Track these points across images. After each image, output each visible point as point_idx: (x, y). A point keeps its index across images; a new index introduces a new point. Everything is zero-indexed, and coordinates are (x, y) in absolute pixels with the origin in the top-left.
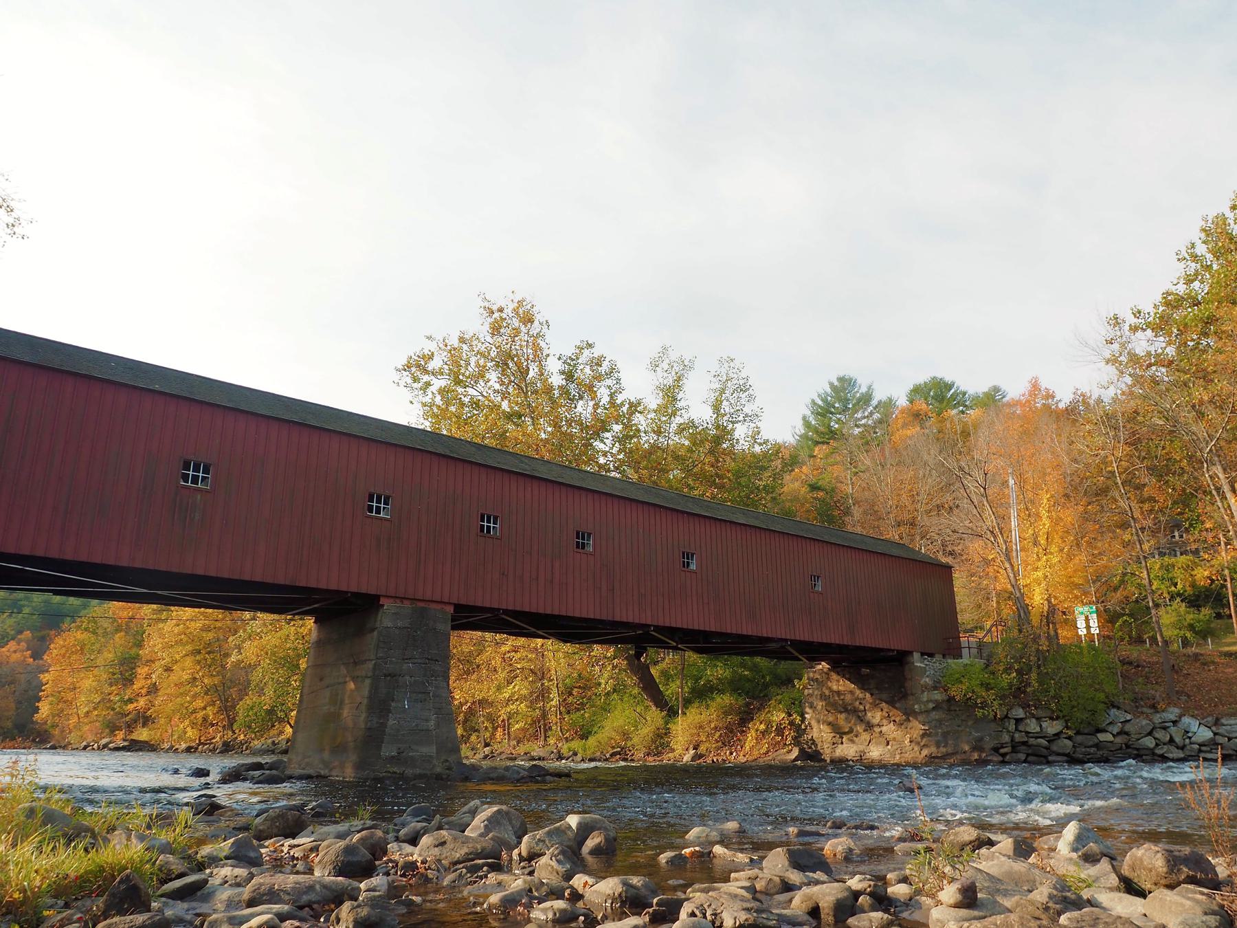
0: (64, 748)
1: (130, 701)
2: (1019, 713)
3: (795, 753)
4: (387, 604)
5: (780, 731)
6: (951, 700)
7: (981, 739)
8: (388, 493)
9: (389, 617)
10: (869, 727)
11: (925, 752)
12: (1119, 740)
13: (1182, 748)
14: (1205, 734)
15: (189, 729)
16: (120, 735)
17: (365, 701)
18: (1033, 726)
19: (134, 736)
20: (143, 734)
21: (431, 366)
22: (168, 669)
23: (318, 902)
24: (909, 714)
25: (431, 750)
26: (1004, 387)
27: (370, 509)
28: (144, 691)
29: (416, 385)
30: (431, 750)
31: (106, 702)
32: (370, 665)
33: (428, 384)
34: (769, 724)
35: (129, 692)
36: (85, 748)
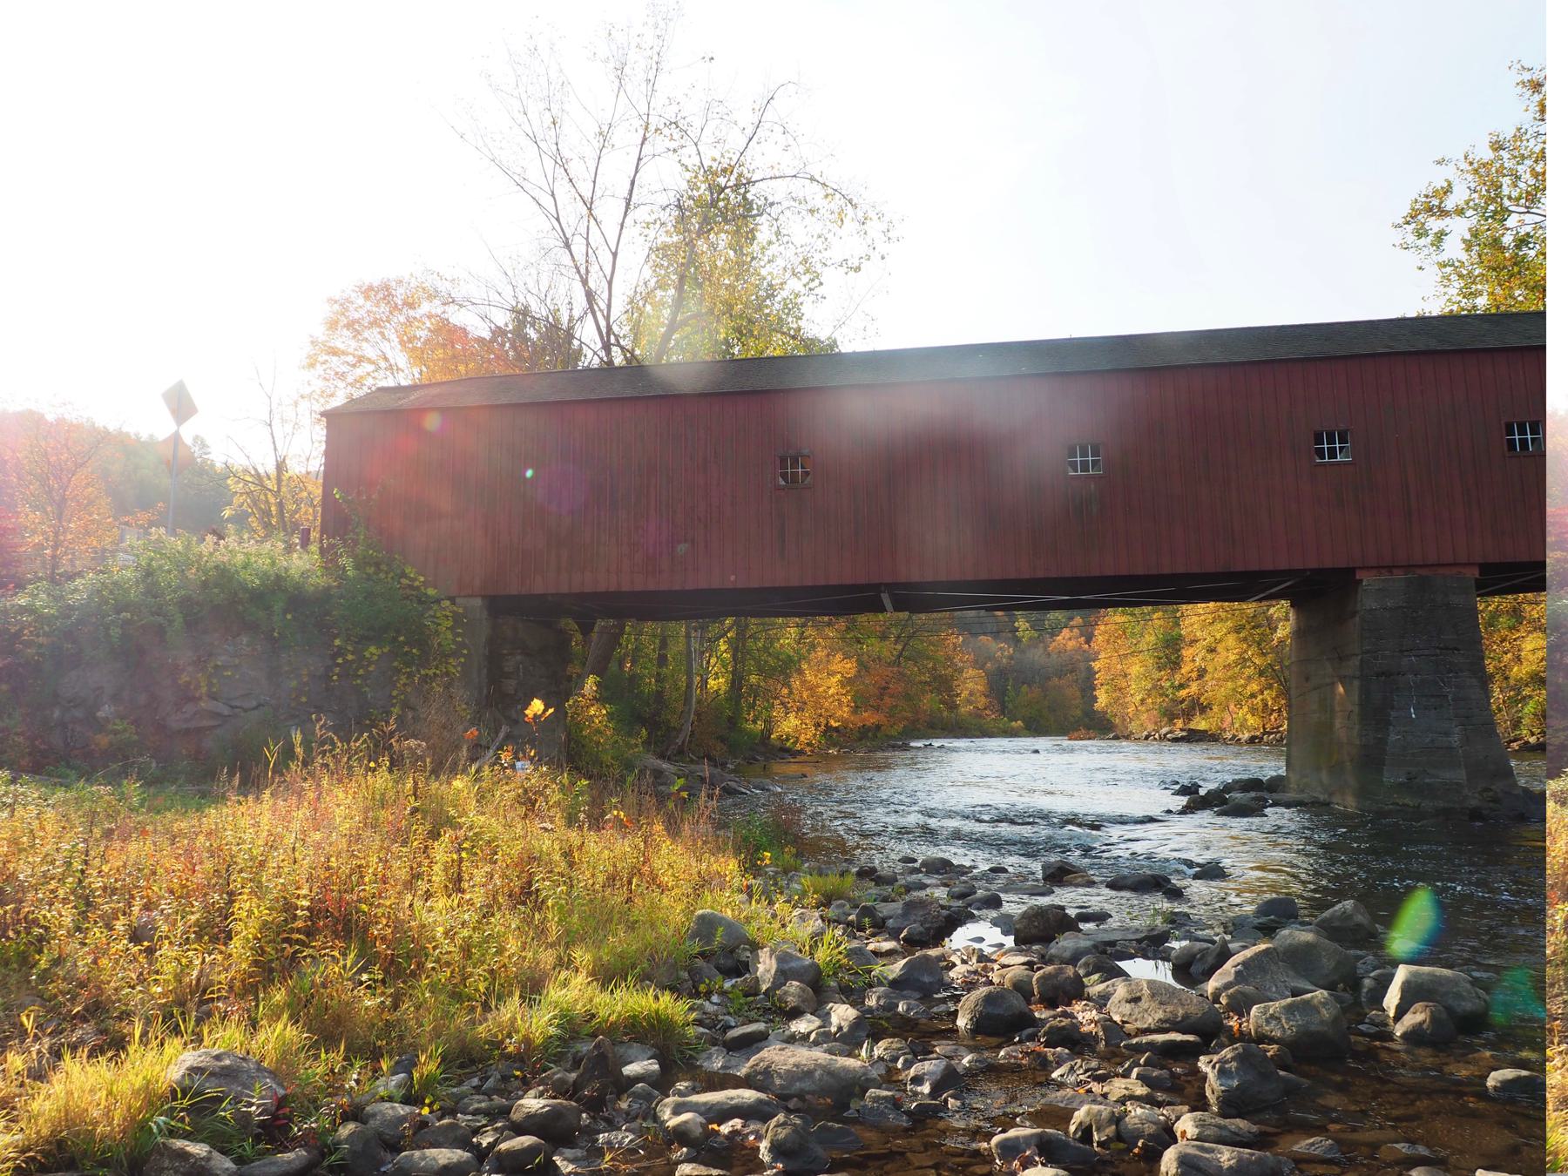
0: (1127, 738)
1: (1182, 686)
4: (1367, 579)
8: (1342, 426)
9: (1374, 594)
15: (1249, 716)
16: (1180, 723)
17: (1356, 709)
19: (1192, 726)
20: (1200, 724)
21: (1450, 204)
22: (1212, 650)
23: (812, 1093)
25: (1461, 775)
27: (1320, 453)
28: (1194, 675)
29: (1423, 241)
30: (1461, 775)
31: (1157, 688)
32: (1356, 661)
33: (1441, 235)
35: (1178, 677)
36: (1147, 738)
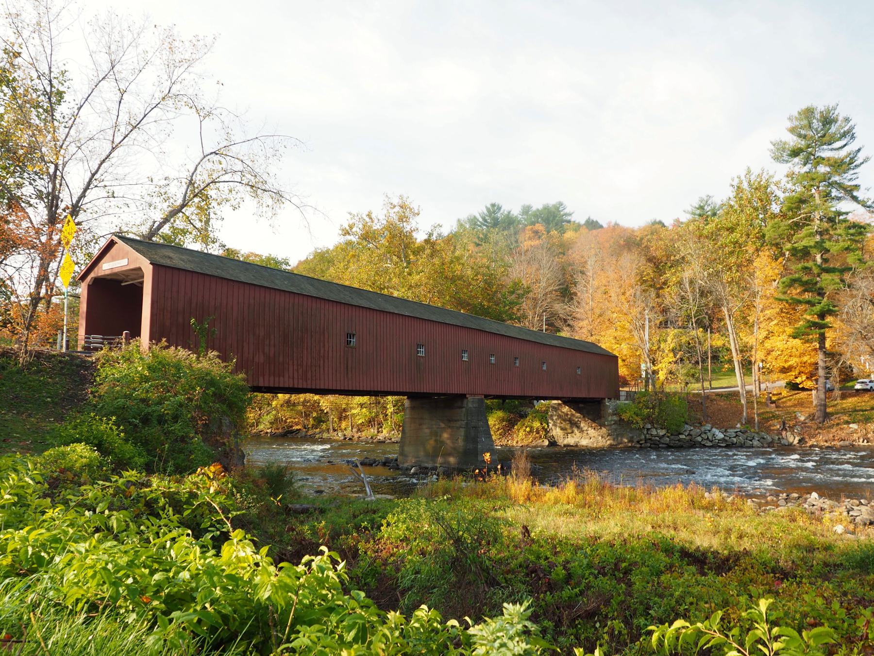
2: (649, 426)
3: (546, 443)
4: (470, 398)
5: (538, 432)
6: (621, 420)
7: (632, 437)
10: (582, 431)
11: (609, 442)
12: (688, 438)
13: (711, 441)
14: (721, 436)
18: (654, 432)
24: (602, 425)
26: (565, 203)
34: (531, 427)
